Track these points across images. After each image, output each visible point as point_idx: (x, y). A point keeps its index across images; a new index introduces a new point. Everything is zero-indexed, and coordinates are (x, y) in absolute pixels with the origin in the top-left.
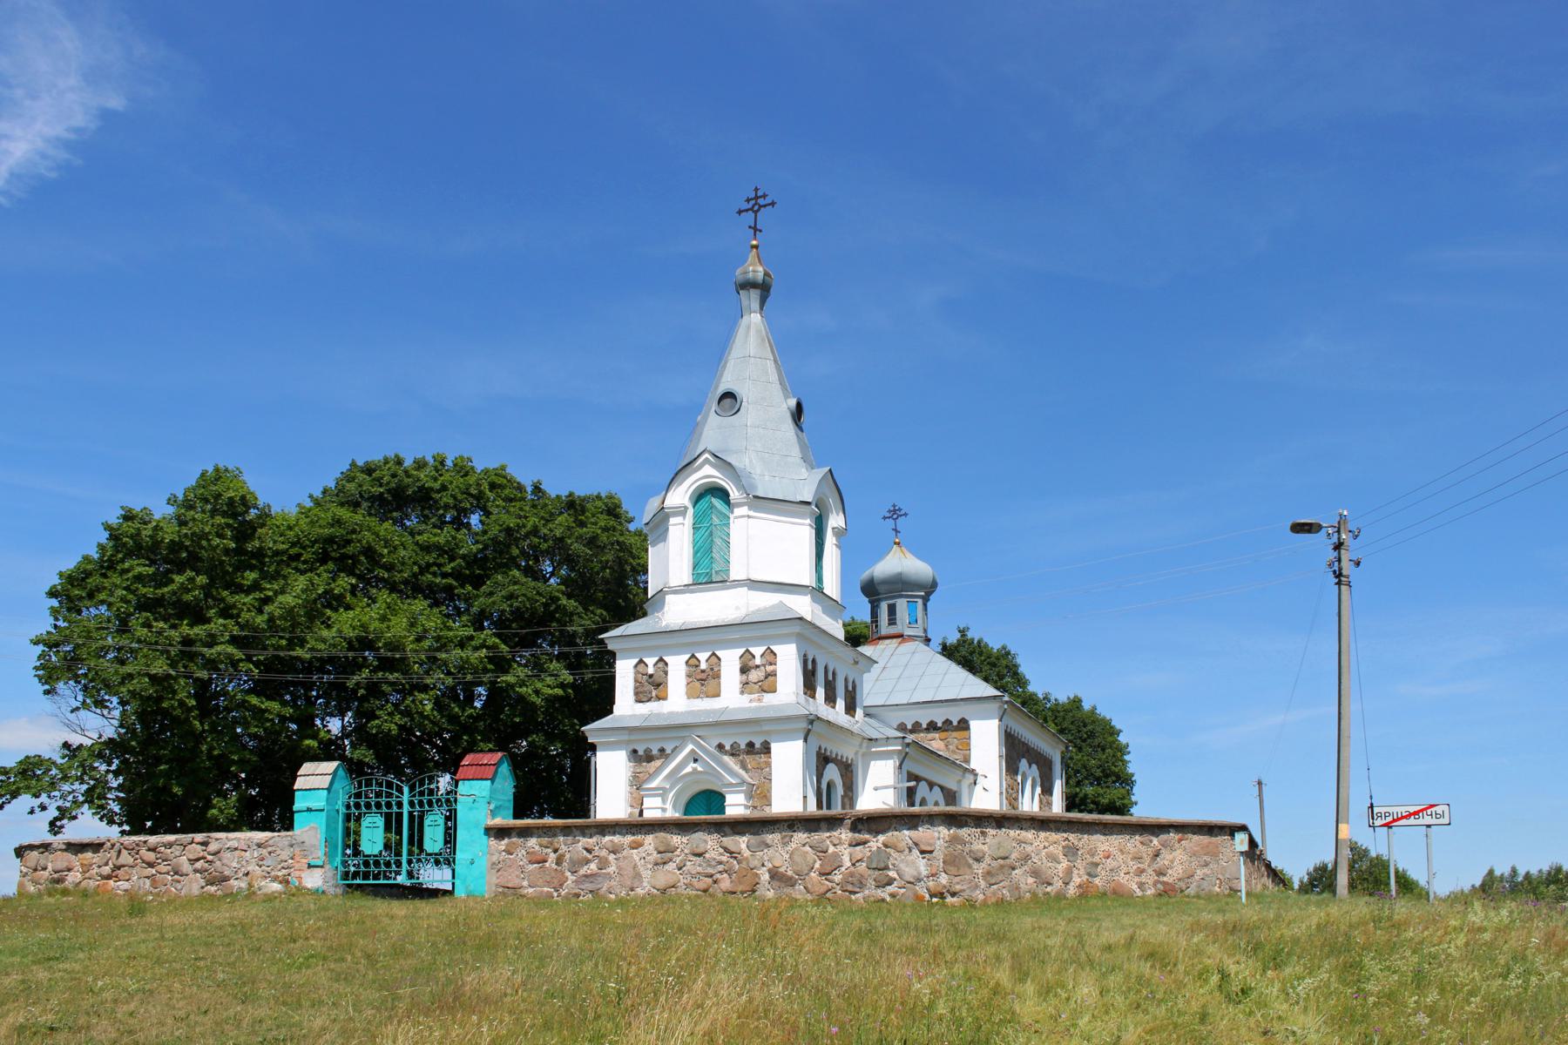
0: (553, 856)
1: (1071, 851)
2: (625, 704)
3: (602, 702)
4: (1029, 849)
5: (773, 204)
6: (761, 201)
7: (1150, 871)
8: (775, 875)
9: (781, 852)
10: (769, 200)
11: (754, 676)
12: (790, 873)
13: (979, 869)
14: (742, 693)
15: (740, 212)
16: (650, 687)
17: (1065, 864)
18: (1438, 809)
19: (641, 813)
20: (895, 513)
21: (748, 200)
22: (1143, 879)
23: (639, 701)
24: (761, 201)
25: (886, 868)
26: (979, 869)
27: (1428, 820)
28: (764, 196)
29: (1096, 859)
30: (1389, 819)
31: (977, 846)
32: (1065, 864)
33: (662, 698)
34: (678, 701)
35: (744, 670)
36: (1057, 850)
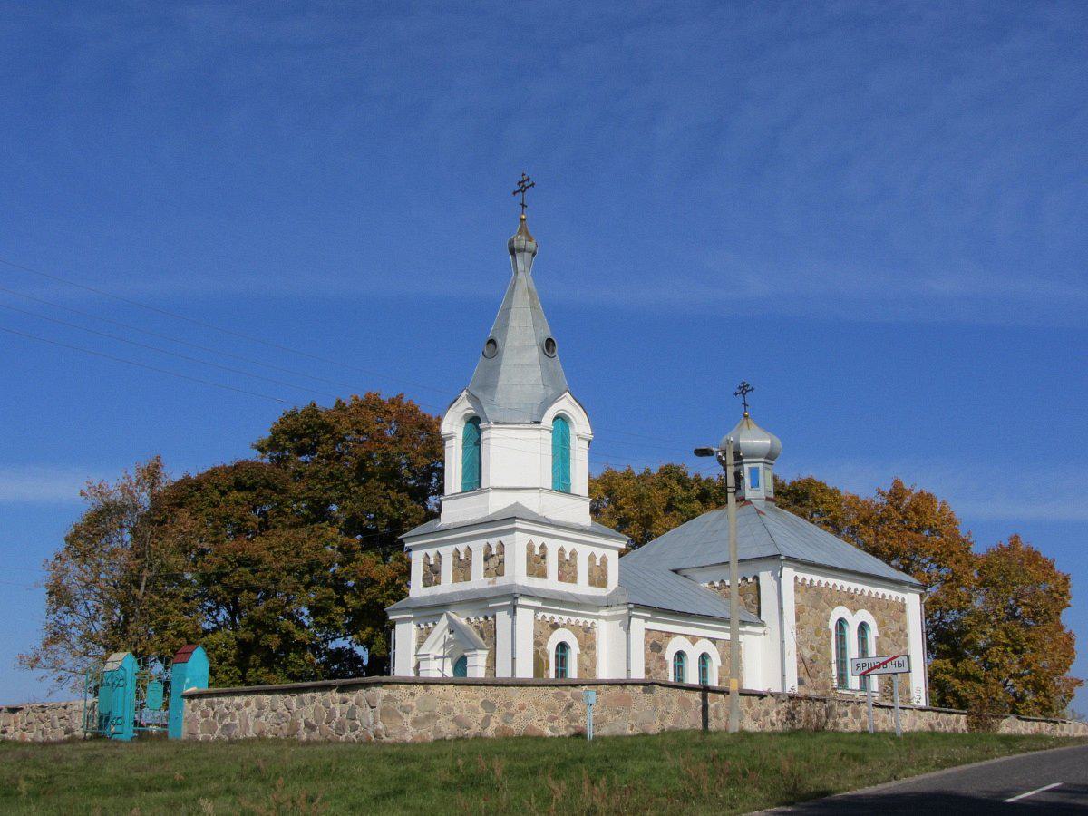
0: (212, 712)
1: (488, 705)
2: (417, 589)
3: (399, 593)
4: (451, 704)
5: (533, 185)
6: (527, 184)
7: (563, 718)
8: (307, 725)
9: (517, 695)
10: (530, 183)
11: (493, 563)
12: (313, 722)
13: (408, 719)
14: (485, 577)
15: (515, 193)
16: (432, 575)
17: (483, 714)
18: (900, 660)
19: (418, 674)
20: (744, 389)
21: (519, 183)
22: (555, 724)
23: (425, 586)
24: (527, 184)
25: (355, 719)
26: (408, 719)
27: (893, 669)
28: (528, 179)
29: (512, 710)
30: (866, 669)
31: (409, 702)
32: (483, 714)
33: (437, 583)
34: (447, 585)
35: (486, 559)
36: (477, 704)
